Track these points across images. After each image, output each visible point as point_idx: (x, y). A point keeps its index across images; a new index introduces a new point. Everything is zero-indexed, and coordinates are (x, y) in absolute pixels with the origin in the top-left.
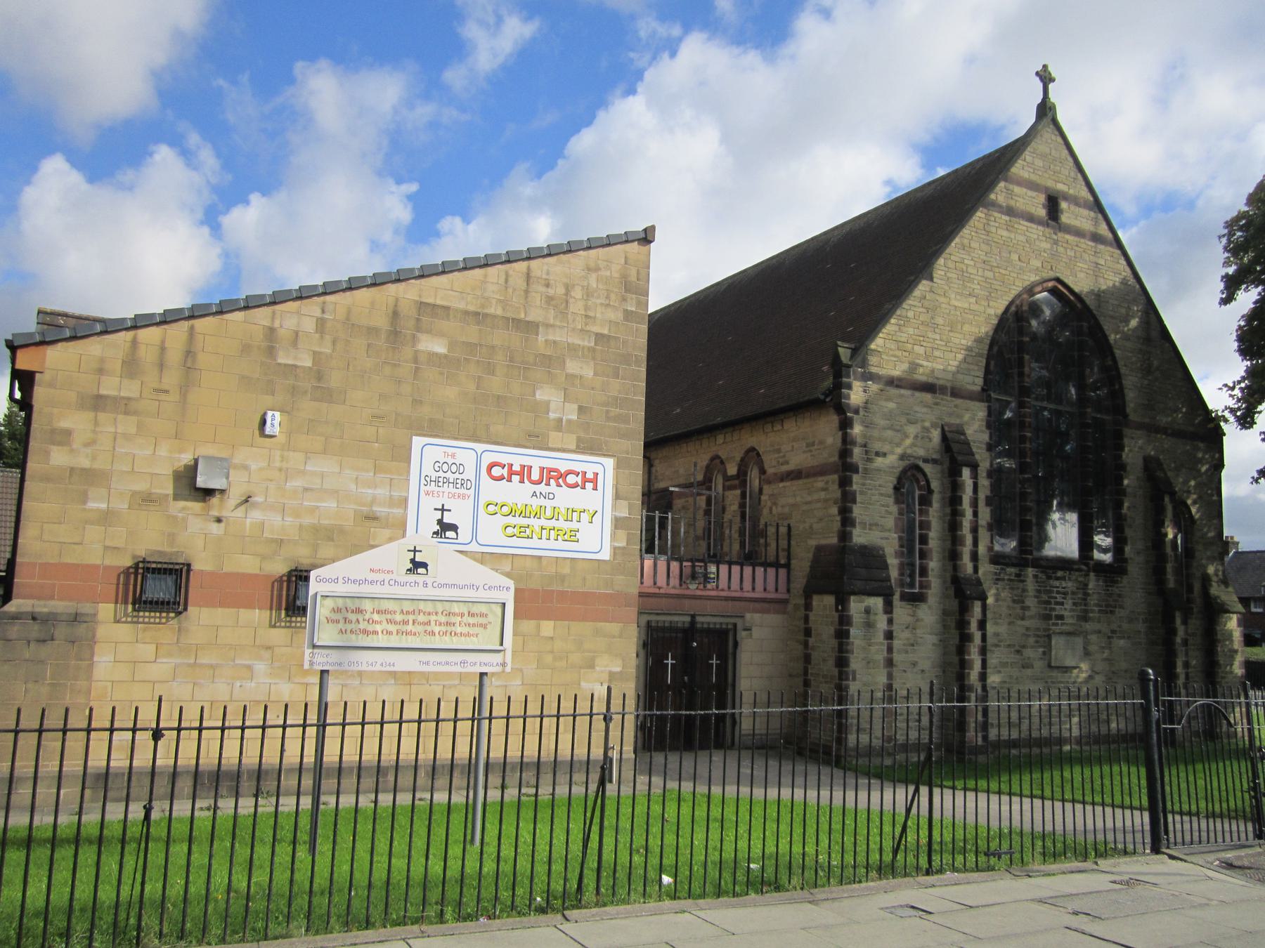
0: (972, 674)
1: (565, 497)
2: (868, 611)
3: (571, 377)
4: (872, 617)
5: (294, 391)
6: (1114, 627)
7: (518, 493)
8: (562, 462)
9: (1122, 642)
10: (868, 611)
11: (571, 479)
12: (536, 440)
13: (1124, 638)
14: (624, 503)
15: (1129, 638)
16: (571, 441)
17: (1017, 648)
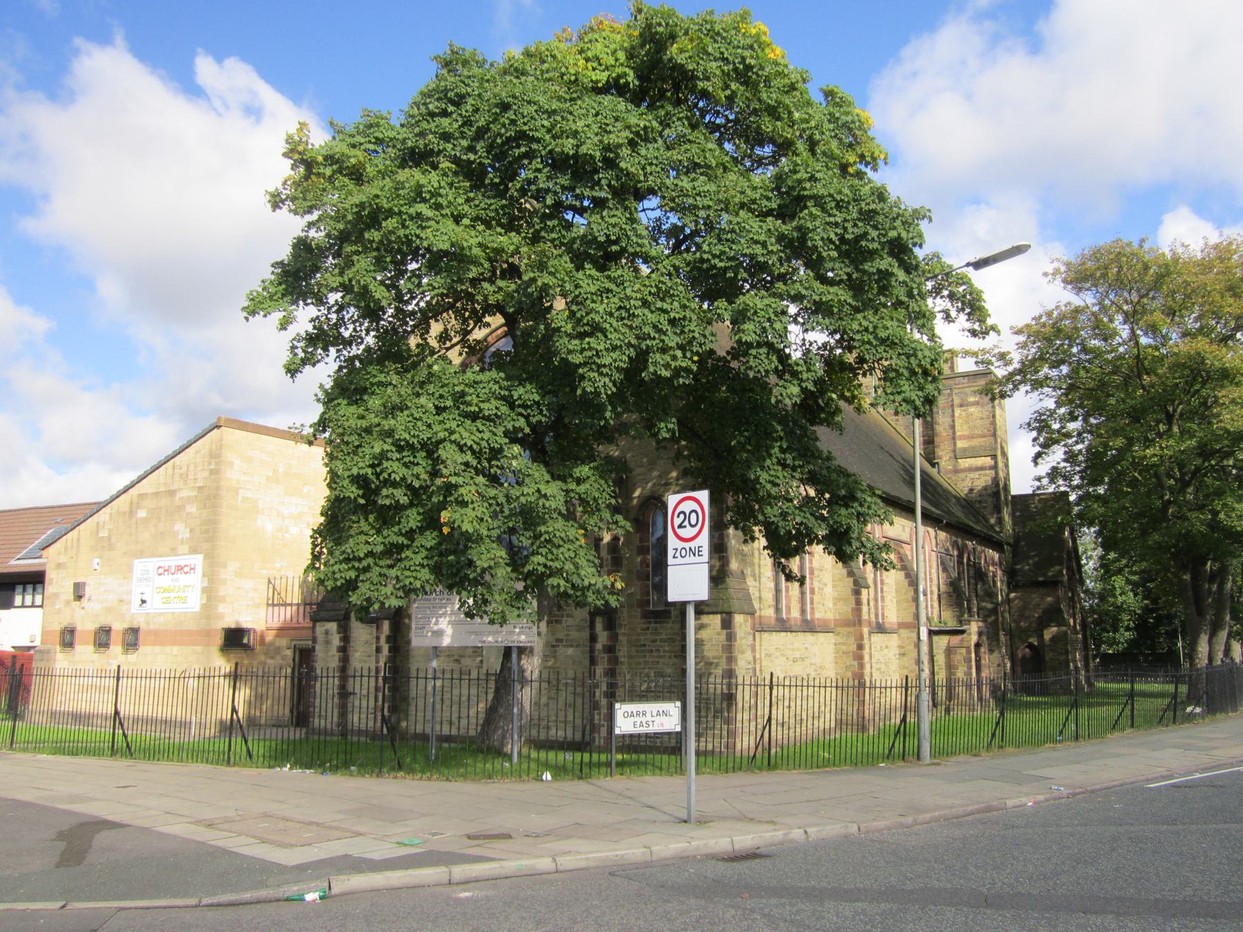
0: (605, 639)
1: (183, 579)
2: (327, 633)
3: (188, 514)
4: (330, 637)
5: (103, 548)
6: (560, 635)
7: (166, 580)
8: (181, 561)
9: (570, 651)
10: (327, 633)
11: (186, 569)
12: (174, 552)
13: (572, 646)
14: (206, 579)
15: (577, 646)
16: (186, 548)
17: (456, 657)
